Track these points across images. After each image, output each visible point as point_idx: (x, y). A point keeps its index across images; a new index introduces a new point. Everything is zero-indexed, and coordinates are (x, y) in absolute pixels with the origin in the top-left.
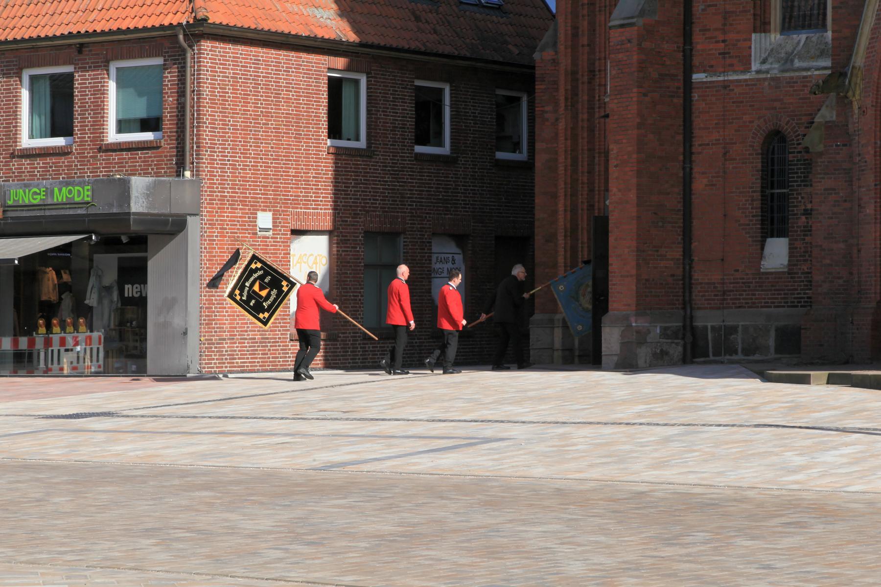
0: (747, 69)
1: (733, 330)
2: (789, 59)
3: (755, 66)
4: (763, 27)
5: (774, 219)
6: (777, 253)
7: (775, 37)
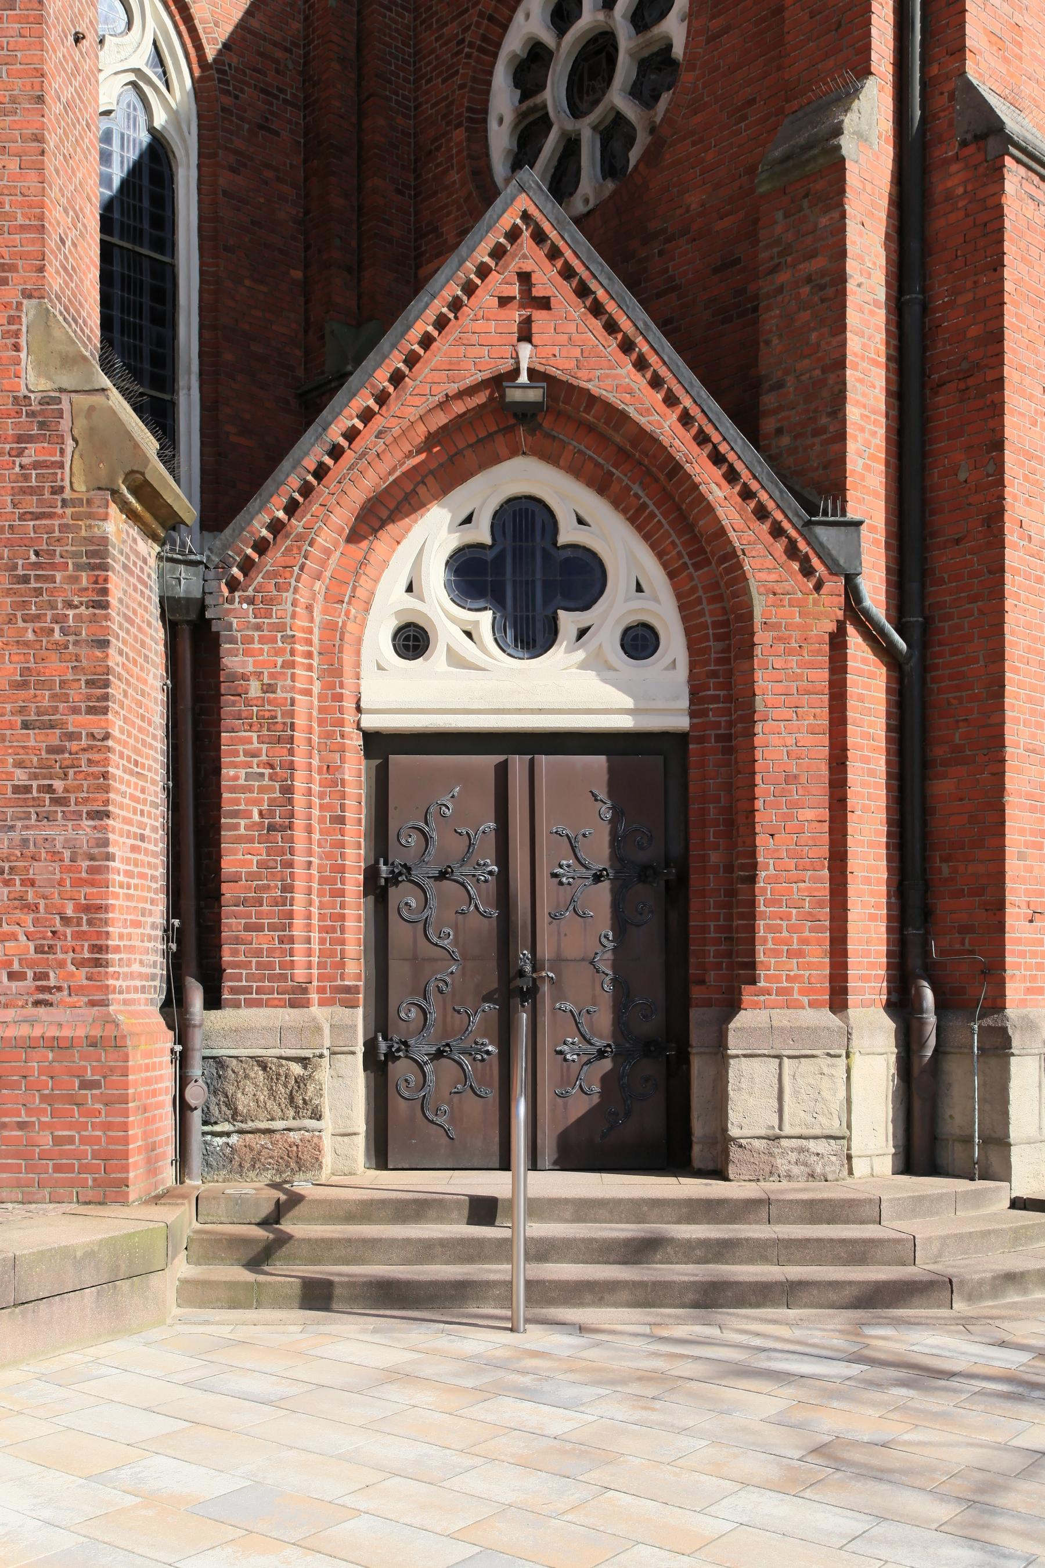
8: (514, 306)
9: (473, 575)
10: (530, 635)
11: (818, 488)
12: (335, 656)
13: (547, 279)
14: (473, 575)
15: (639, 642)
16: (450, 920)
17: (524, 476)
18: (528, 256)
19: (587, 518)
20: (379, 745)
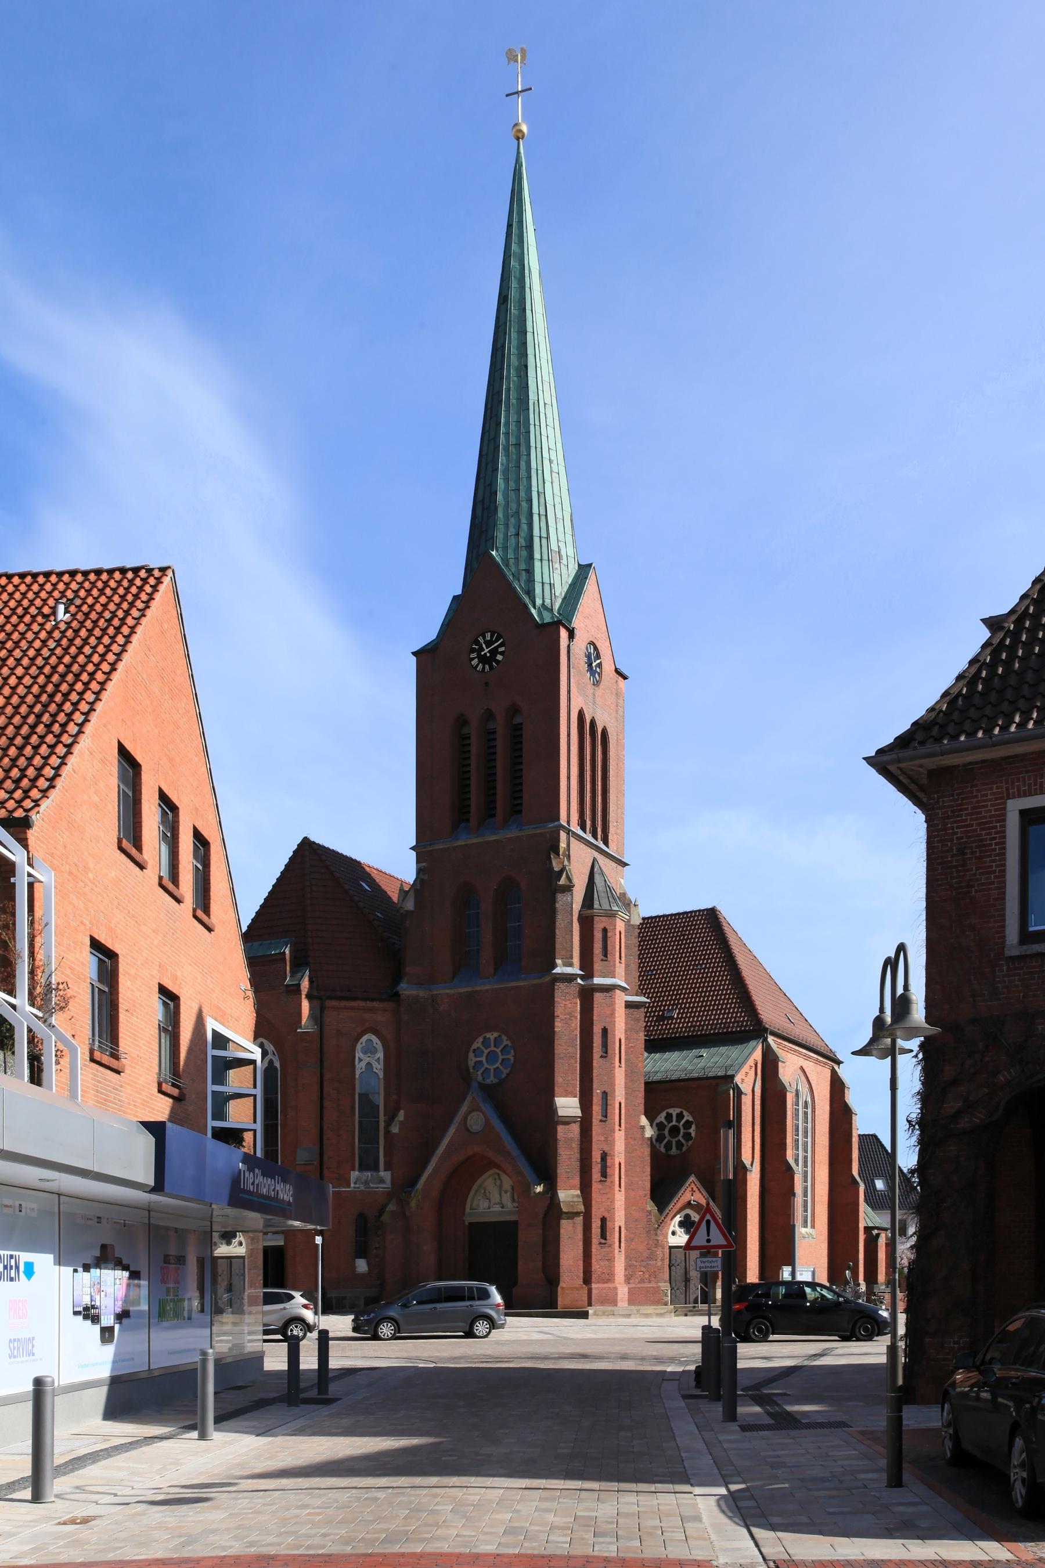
0: (349, 1186)
1: (345, 1298)
2: (366, 1183)
4: (354, 1170)
5: (361, 1251)
6: (362, 1266)
7: (357, 1173)
8: (691, 1193)
9: (681, 1224)
12: (666, 1237)
13: (695, 1189)
14: (681, 1224)
16: (679, 1271)
17: (688, 1211)
18: (693, 1186)
20: (671, 1248)
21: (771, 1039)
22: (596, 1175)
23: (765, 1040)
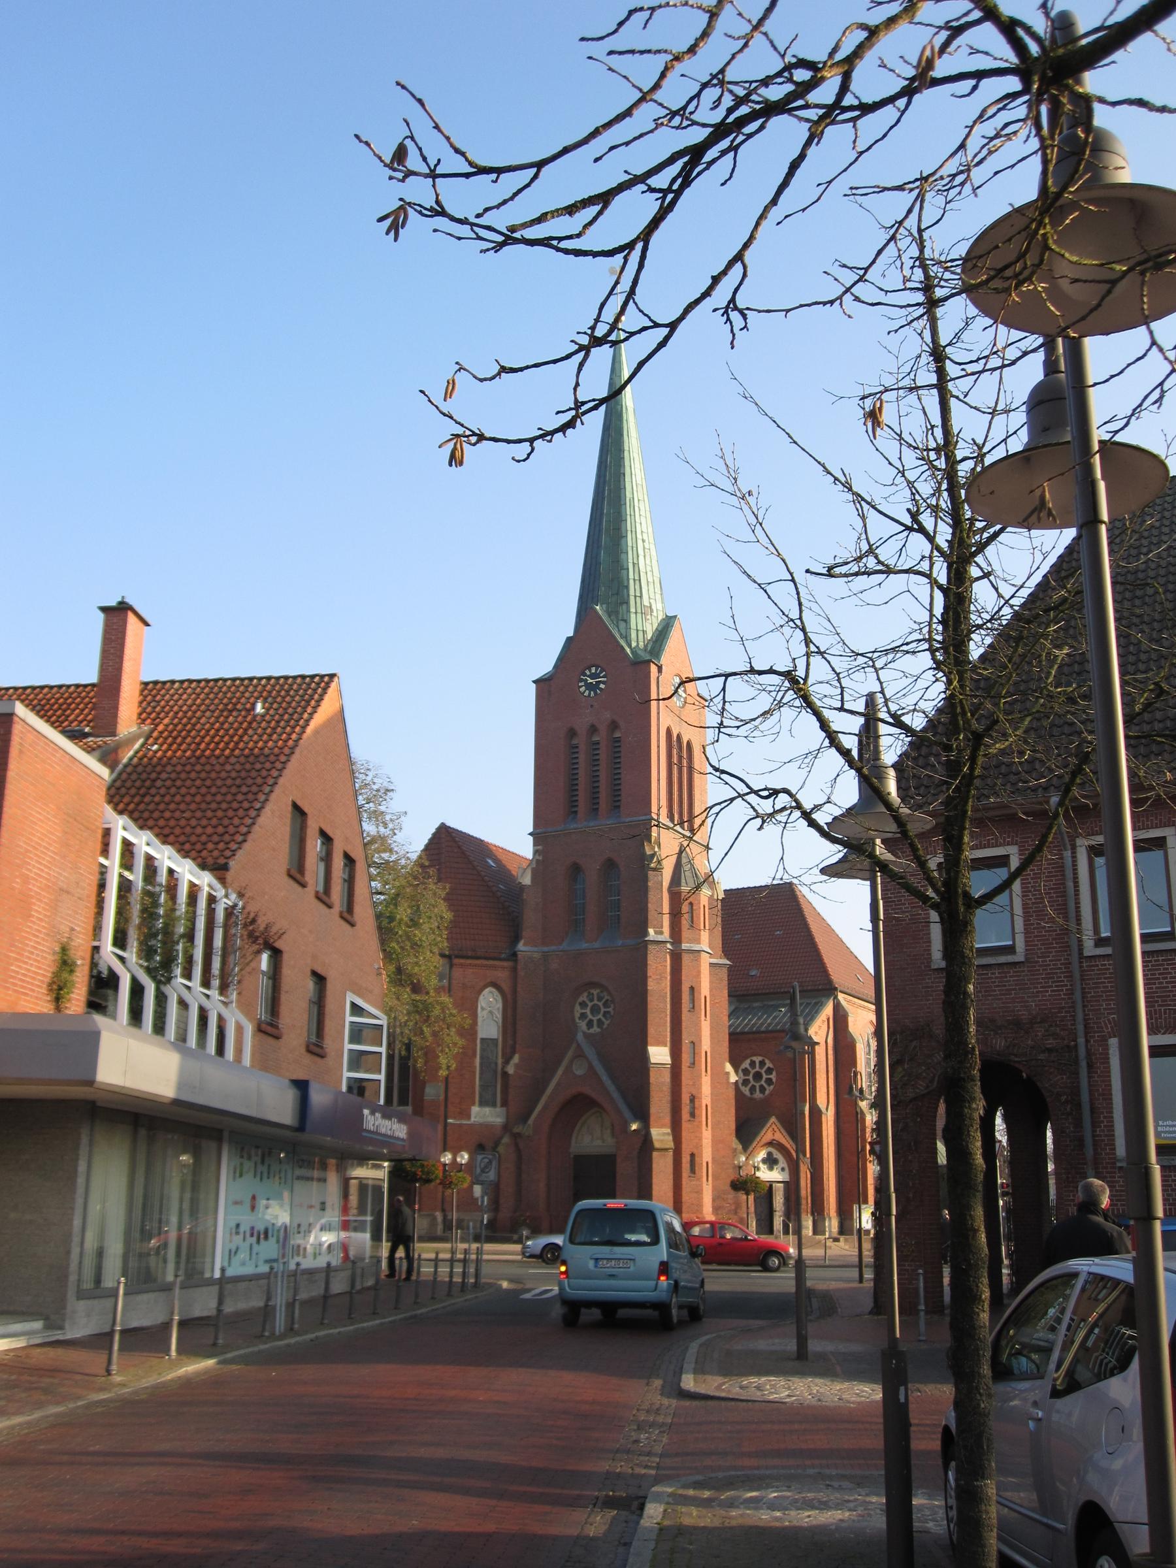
3: (473, 1119)
8: (773, 1131)
10: (771, 1169)
11: (800, 1150)
15: (783, 1169)
19: (777, 1155)
21: (841, 996)
22: (685, 1115)
23: (836, 997)
